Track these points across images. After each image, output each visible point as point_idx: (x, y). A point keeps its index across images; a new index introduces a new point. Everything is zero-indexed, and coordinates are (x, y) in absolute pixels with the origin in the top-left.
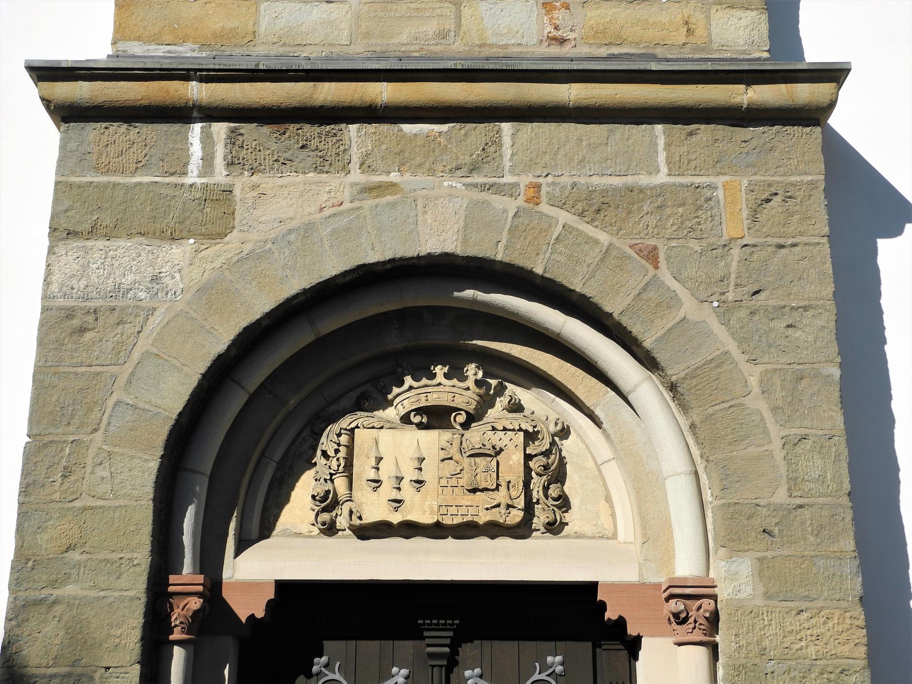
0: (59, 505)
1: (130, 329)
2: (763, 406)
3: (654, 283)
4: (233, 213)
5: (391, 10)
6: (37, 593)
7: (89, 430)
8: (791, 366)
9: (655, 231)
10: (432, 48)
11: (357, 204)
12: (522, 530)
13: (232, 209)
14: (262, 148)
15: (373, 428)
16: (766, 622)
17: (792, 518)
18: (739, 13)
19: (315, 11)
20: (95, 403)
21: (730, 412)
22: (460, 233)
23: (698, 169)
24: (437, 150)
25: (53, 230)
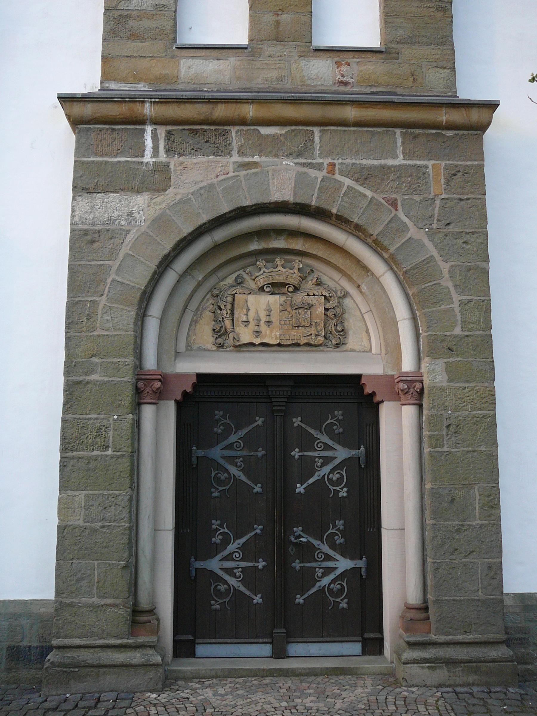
0: (87, 334)
1: (116, 241)
2: (450, 284)
4: (170, 178)
5: (252, 64)
6: (77, 378)
7: (99, 294)
8: (465, 264)
9: (396, 190)
10: (275, 86)
11: (236, 173)
13: (169, 176)
14: (184, 142)
15: (245, 294)
16: (448, 394)
17: (462, 342)
19: (211, 65)
20: (102, 281)
21: (433, 287)
22: (293, 190)
23: (419, 157)
24: (279, 144)
25: (75, 187)
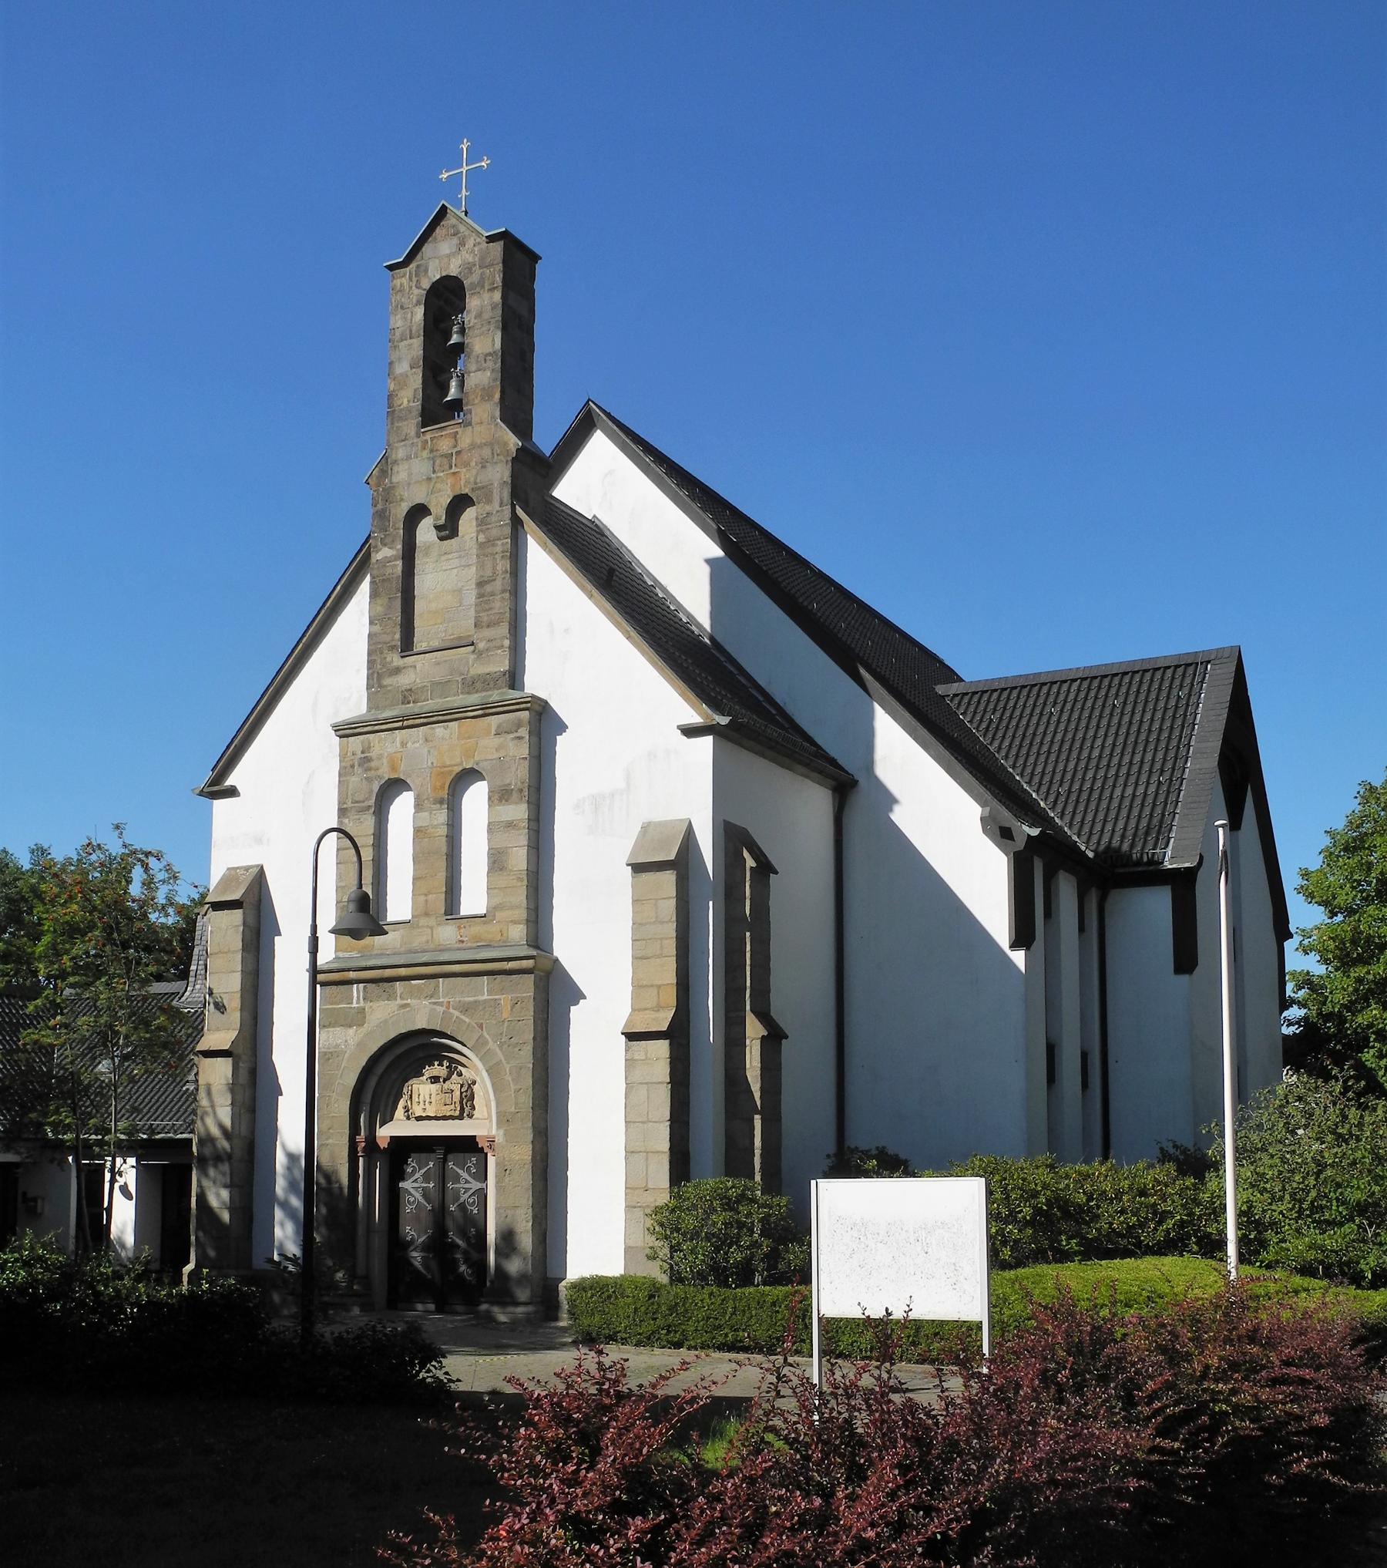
3: (481, 1036)
12: (460, 1117)
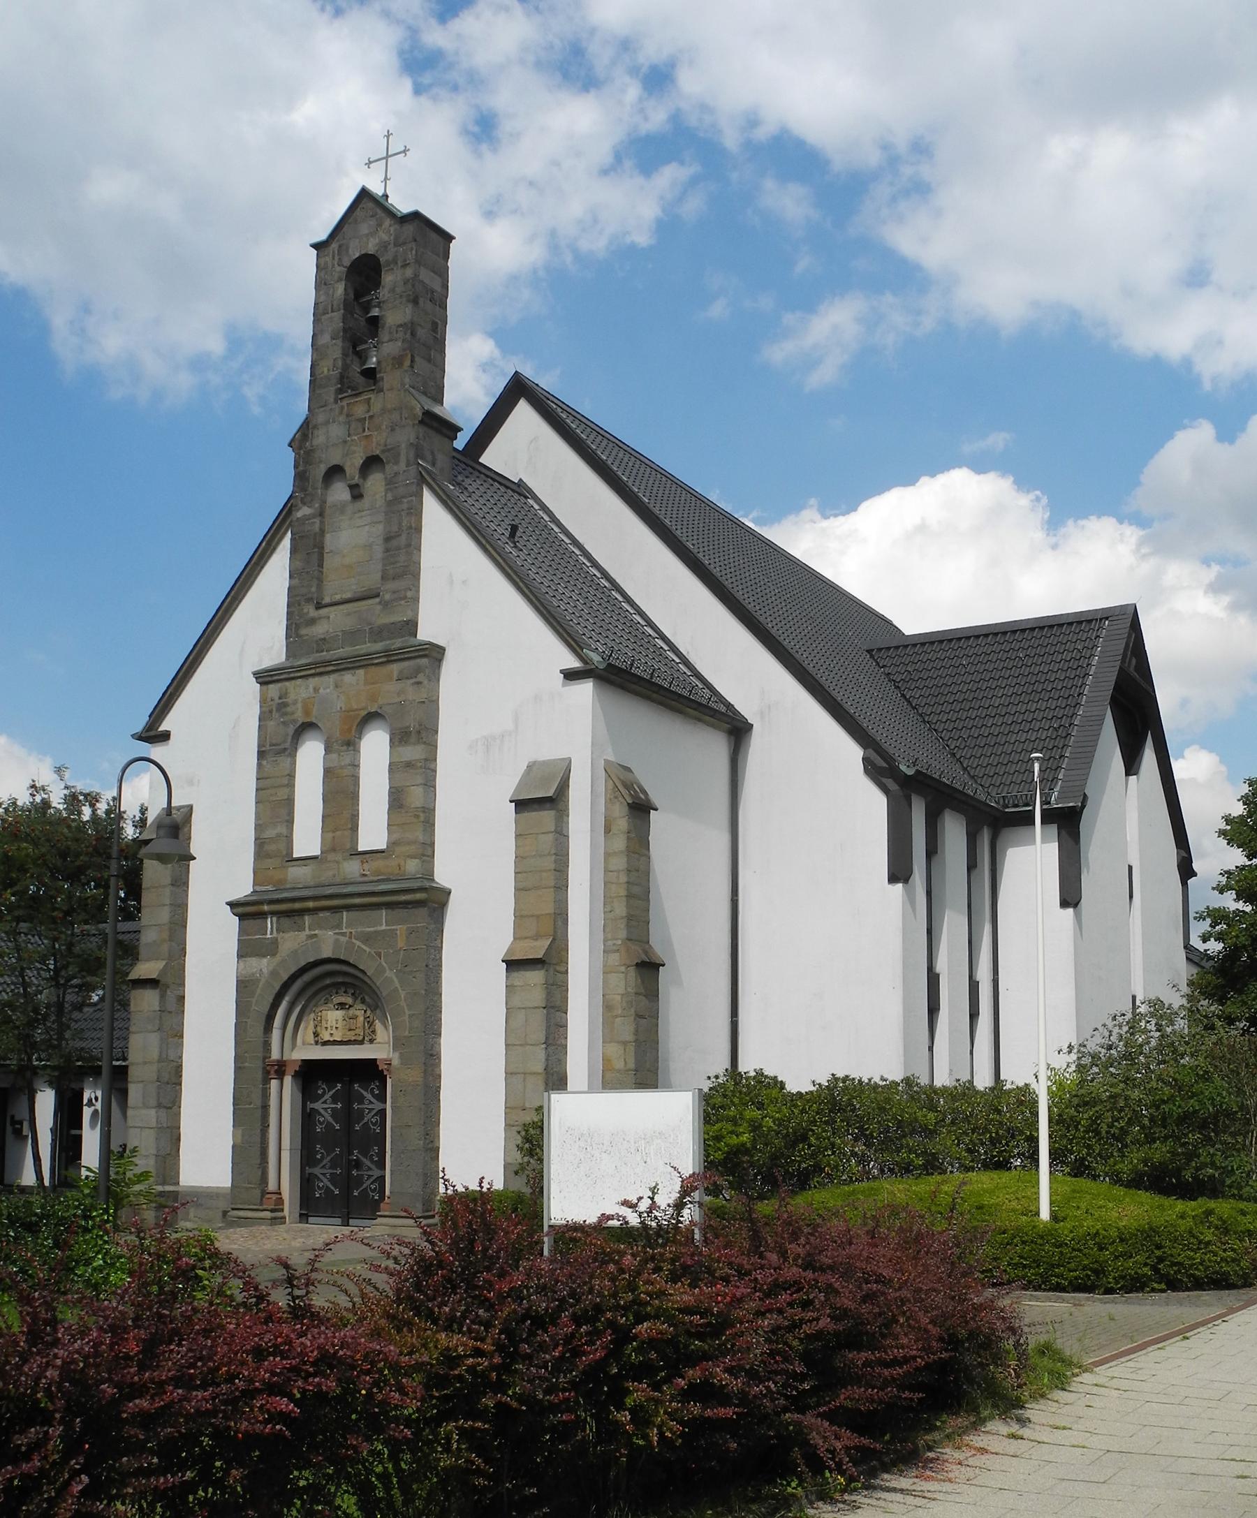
18: (413, 860)
